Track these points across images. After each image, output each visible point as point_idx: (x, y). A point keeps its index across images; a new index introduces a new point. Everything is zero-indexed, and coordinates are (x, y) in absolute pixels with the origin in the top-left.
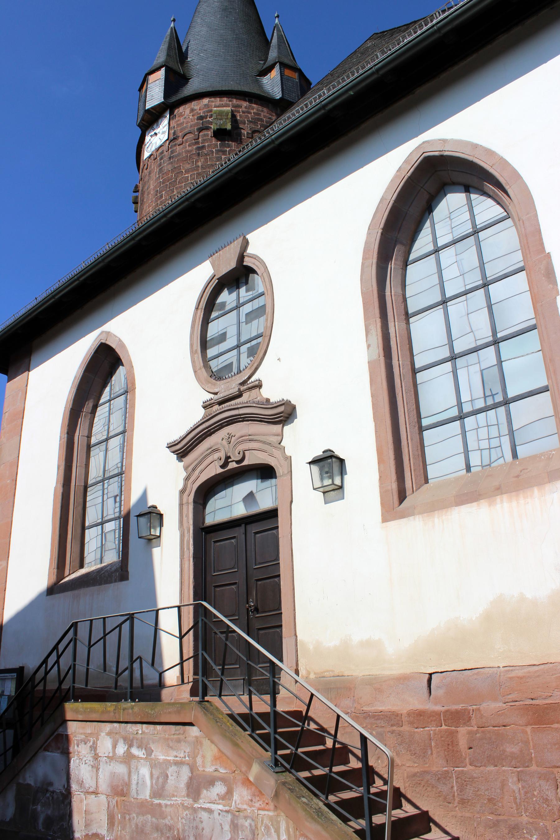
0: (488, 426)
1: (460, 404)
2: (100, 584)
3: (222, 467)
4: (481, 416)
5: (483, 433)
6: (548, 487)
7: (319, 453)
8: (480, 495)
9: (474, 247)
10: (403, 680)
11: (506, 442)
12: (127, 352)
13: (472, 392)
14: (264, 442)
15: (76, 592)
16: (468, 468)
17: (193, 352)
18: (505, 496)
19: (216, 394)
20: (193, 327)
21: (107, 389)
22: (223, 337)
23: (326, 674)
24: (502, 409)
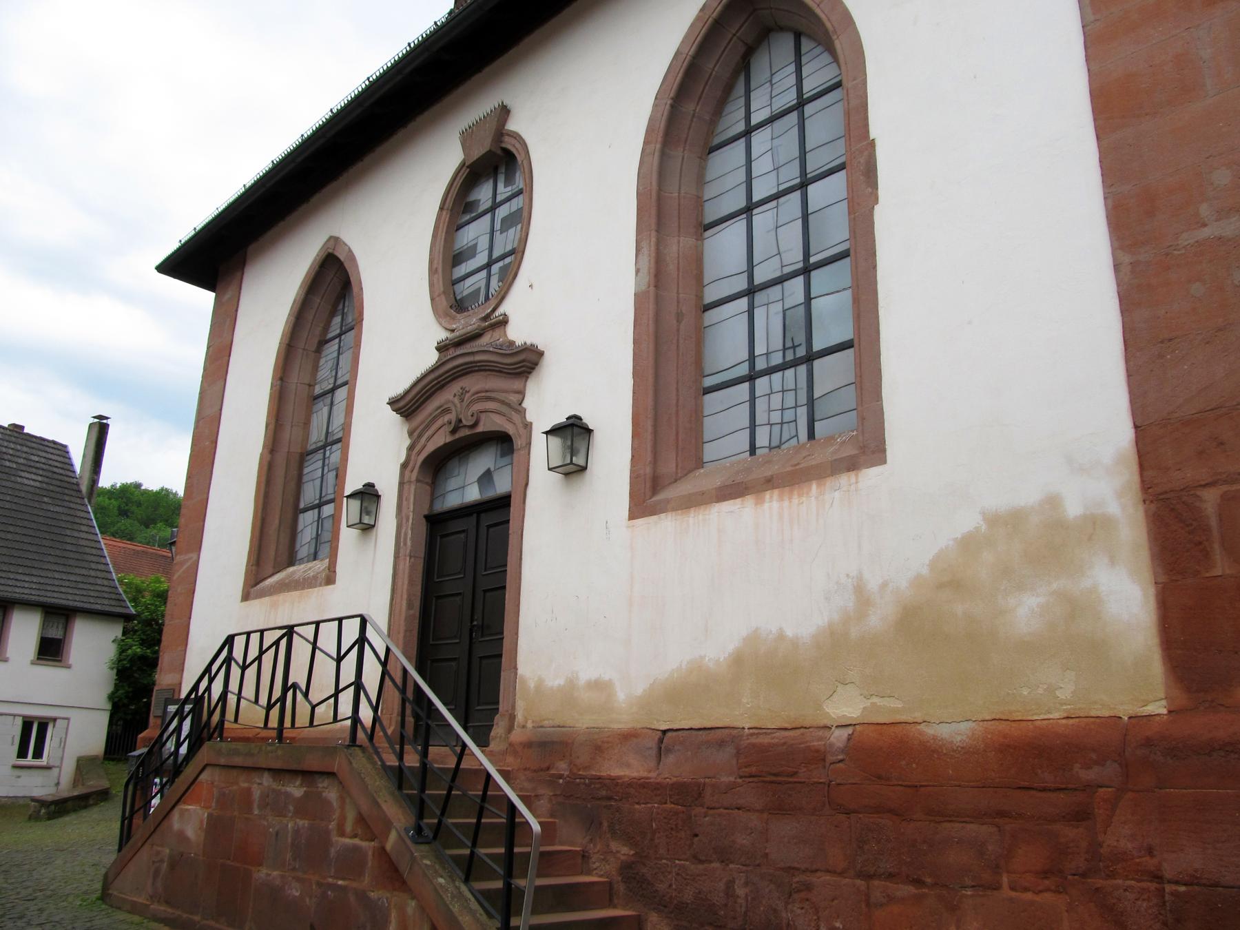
0: (783, 391)
1: (752, 357)
2: (303, 589)
3: (453, 432)
4: (777, 377)
5: (776, 400)
6: (830, 482)
7: (562, 419)
8: (746, 488)
9: (796, 128)
10: (628, 736)
11: (802, 412)
12: (357, 266)
13: (769, 338)
14: (503, 402)
15: (275, 598)
16: (753, 449)
17: (432, 271)
18: (776, 492)
19: (453, 331)
20: (434, 236)
21: (337, 320)
22: (471, 252)
23: (546, 723)
24: (802, 369)
